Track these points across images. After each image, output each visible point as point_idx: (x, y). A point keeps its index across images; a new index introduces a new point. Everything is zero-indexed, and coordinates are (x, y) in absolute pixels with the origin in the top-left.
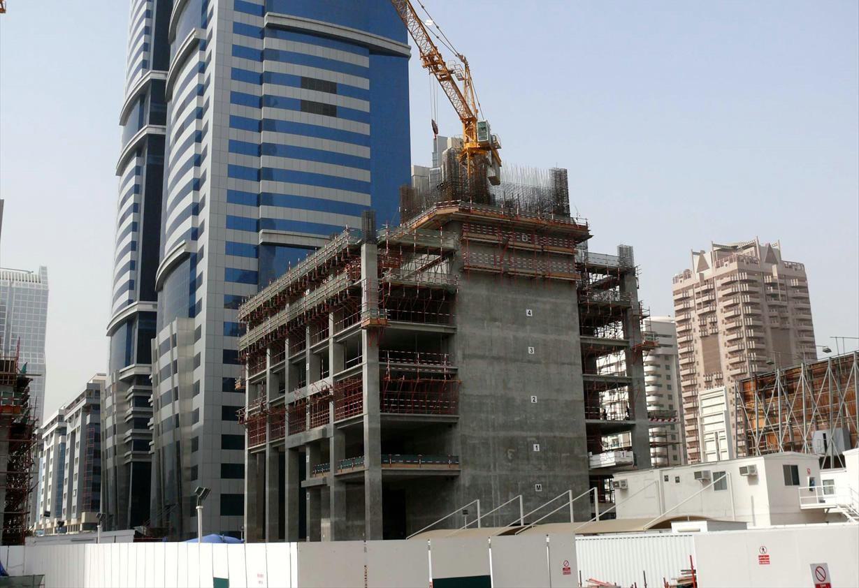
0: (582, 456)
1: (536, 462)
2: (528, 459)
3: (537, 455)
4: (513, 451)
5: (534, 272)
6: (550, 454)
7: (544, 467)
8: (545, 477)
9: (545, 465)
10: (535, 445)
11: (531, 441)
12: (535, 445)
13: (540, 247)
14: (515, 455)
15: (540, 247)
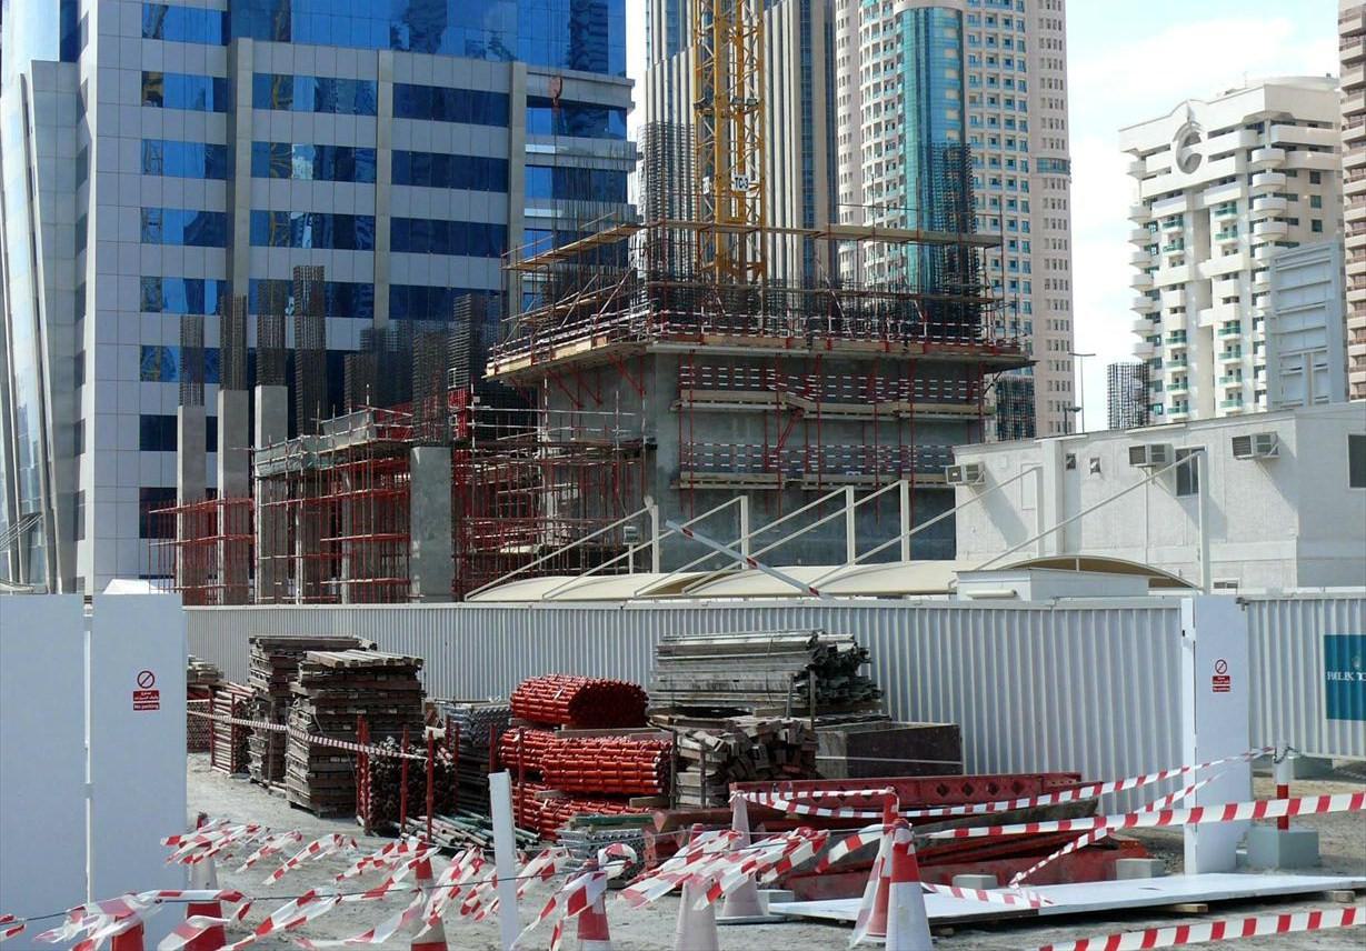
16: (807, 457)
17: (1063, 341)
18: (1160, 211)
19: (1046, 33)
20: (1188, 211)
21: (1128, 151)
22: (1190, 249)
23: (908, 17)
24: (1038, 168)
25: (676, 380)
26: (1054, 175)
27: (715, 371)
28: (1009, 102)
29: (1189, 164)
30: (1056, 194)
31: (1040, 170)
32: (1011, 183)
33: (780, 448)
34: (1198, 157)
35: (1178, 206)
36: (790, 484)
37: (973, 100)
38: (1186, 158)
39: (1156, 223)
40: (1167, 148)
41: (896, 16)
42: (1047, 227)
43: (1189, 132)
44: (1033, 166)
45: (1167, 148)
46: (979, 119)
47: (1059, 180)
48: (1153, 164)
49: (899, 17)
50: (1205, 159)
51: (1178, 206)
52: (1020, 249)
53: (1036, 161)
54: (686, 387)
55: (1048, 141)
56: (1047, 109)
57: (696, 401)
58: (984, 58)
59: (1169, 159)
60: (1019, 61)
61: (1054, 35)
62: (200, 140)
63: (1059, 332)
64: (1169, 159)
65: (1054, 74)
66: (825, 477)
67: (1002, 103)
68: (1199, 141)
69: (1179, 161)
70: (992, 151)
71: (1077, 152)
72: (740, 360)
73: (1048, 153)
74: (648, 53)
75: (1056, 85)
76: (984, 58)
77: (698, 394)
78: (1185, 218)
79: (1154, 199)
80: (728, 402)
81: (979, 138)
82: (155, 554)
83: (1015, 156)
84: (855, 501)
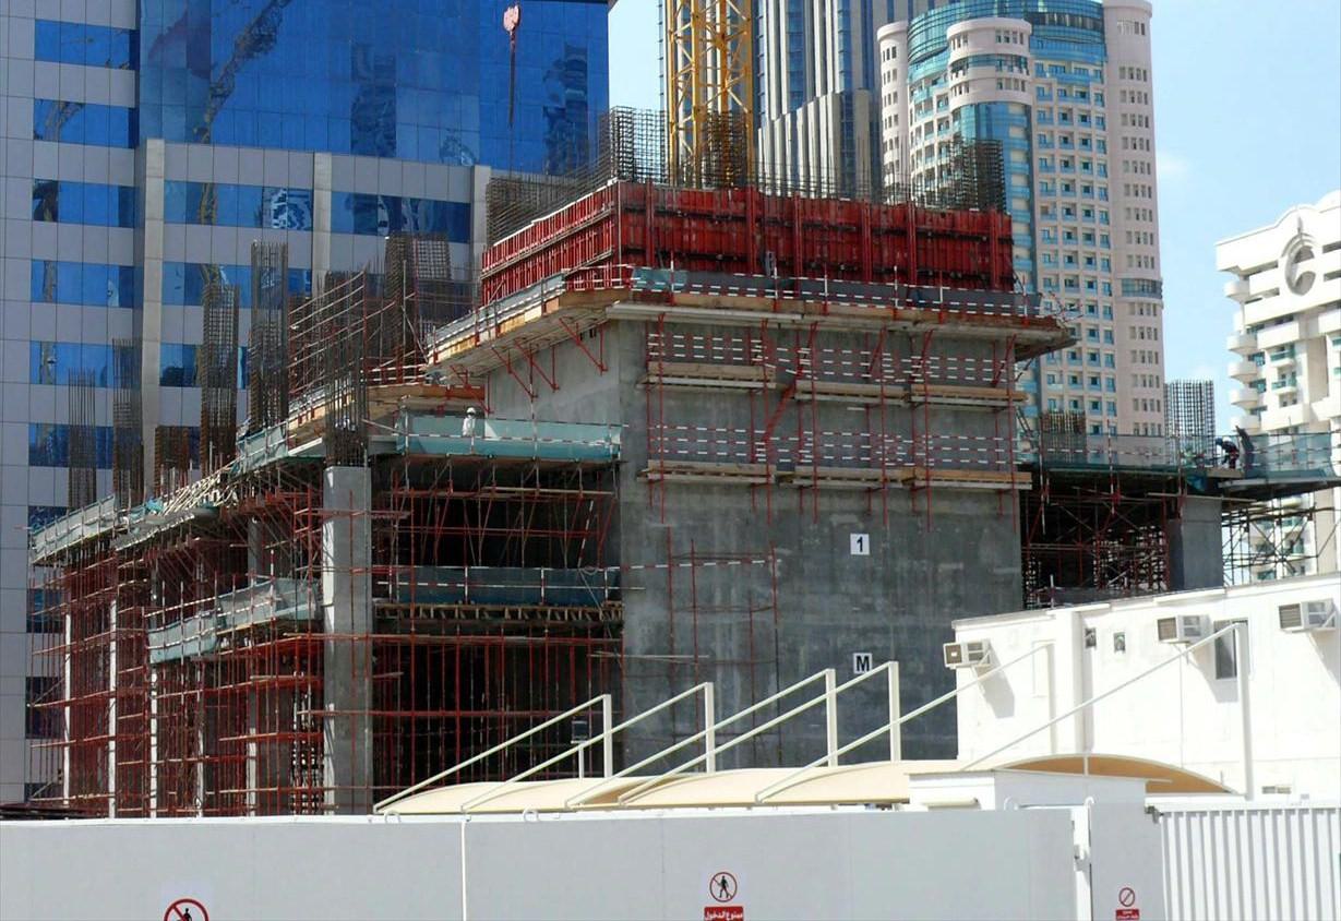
0: (1006, 570)
1: (854, 588)
2: (833, 579)
3: (864, 571)
4: (787, 552)
5: (876, 472)
6: (903, 564)
7: (880, 602)
8: (885, 630)
9: (886, 595)
10: (854, 538)
11: (841, 525)
12: (854, 538)
13: (899, 391)
14: (792, 569)
15: (899, 391)
16: (800, 445)
17: (1139, 93)
18: (1269, 339)
19: (1131, 132)
20: (1300, 341)
21: (1227, 270)
22: (1303, 380)
23: (968, 116)
24: (1123, 292)
25: (644, 351)
26: (1142, 299)
27: (688, 340)
28: (1089, 237)
29: (1300, 285)
30: (1147, 321)
31: (1125, 293)
32: (1094, 357)
33: (730, 187)
34: (1310, 276)
35: (1289, 333)
36: (780, 479)
37: (1045, 211)
38: (1297, 276)
39: (1262, 354)
40: (1275, 265)
41: (953, 113)
42: (1136, 385)
43: (1300, 246)
44: (1117, 288)
45: (1275, 265)
46: (1048, 138)
47: (1149, 304)
48: (1258, 284)
49: (956, 114)
50: (1319, 278)
51: (1289, 333)
52: (1103, 363)
53: (1120, 282)
54: (656, 359)
55: (1132, 212)
56: (1131, 173)
57: (667, 376)
58: (1057, 162)
59: (1276, 278)
60: (1109, 403)
61: (1141, 132)
62: (181, 259)
63: (1147, 365)
64: (1276, 278)
65: (1140, 179)
66: (822, 470)
67: (1081, 237)
68: (1312, 256)
69: (1289, 280)
70: (1067, 272)
71: (1170, 271)
72: (722, 330)
73: (1134, 273)
74: (661, 71)
75: (1145, 240)
76: (1057, 162)
77: (668, 367)
78: (1297, 349)
79: (1260, 326)
80: (705, 378)
81: (1049, 162)
82: (36, 756)
83: (1092, 182)
84: (902, 716)
